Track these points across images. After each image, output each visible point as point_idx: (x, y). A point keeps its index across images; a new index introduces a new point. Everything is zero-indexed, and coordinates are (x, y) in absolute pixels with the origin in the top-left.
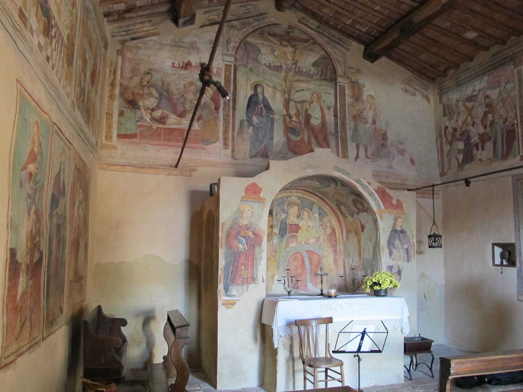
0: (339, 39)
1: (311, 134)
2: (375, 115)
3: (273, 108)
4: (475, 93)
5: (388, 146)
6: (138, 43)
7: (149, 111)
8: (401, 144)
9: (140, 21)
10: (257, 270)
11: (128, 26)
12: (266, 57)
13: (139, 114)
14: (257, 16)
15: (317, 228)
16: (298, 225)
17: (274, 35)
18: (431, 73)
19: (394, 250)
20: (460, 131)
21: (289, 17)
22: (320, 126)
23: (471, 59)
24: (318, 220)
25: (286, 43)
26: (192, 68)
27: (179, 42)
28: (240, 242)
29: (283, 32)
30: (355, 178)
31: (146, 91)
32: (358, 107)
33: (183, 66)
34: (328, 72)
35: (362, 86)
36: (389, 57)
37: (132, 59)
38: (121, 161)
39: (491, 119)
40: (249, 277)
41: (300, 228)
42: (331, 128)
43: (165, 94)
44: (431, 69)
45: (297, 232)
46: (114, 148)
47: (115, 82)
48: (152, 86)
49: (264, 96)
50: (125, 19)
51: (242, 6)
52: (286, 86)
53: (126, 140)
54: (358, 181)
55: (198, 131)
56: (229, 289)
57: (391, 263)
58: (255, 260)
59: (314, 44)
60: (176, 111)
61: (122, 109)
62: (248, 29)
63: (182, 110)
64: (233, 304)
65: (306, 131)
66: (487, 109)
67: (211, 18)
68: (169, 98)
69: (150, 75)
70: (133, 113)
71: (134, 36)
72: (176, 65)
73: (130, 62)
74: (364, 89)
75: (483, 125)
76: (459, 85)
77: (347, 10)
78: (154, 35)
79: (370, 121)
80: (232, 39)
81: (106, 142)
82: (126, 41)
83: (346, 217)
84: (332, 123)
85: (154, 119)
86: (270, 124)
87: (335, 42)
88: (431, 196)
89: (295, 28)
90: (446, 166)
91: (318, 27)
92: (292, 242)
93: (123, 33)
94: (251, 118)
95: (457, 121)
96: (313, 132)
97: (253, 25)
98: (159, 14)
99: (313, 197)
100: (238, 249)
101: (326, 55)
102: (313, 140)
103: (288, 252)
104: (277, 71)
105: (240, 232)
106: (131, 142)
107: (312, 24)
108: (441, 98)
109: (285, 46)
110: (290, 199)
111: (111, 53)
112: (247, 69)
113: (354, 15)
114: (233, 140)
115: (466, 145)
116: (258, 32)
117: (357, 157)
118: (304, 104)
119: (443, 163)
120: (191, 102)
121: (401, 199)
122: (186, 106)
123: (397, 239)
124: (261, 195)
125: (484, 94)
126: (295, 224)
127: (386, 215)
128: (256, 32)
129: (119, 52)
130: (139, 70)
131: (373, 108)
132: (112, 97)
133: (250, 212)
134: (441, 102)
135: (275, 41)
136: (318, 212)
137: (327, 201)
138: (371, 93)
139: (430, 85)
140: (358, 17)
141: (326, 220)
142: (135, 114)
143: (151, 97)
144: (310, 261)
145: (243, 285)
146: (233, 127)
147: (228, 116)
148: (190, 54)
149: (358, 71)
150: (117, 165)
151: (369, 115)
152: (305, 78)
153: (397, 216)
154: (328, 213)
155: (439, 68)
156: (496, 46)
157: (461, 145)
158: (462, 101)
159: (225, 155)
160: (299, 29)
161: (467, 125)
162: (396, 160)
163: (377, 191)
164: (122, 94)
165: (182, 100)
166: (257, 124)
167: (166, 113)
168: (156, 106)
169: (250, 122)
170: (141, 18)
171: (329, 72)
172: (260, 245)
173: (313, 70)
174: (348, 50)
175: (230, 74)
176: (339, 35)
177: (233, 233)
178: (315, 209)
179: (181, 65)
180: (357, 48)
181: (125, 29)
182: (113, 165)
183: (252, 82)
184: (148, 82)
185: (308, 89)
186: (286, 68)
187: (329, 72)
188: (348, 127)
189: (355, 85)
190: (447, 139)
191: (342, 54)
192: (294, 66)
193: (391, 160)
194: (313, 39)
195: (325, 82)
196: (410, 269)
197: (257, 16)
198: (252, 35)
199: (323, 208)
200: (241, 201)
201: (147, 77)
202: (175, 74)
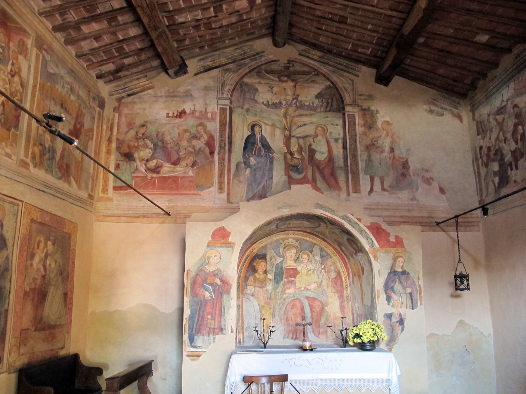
0: (346, 66)
1: (316, 169)
2: (393, 142)
3: (272, 147)
4: (504, 104)
5: (410, 175)
6: (133, 98)
7: (144, 162)
8: (427, 171)
9: (135, 78)
11: (126, 83)
12: (264, 95)
13: (134, 165)
14: (254, 55)
15: (319, 272)
16: (296, 269)
18: (458, 86)
19: (393, 295)
20: (493, 150)
21: (290, 52)
22: (327, 160)
23: (496, 65)
24: (319, 263)
25: (285, 78)
26: (187, 115)
27: (173, 92)
29: (281, 68)
30: (341, 214)
31: (141, 143)
32: (371, 136)
33: (177, 115)
35: (375, 112)
36: (405, 75)
37: (128, 114)
38: (116, 212)
39: (522, 131)
40: (216, 327)
41: (298, 273)
42: (339, 162)
43: (160, 144)
44: (456, 84)
45: (295, 277)
46: (110, 199)
47: (111, 138)
48: (147, 138)
49: (262, 135)
50: (119, 78)
51: (238, 48)
52: (287, 123)
53: (121, 191)
54: (345, 218)
55: (192, 177)
56: (195, 340)
57: (389, 310)
58: (223, 309)
59: (317, 75)
60: (170, 159)
62: (244, 70)
63: (177, 157)
64: (199, 356)
66: (516, 121)
67: (206, 64)
68: (164, 147)
70: (128, 165)
71: (130, 92)
72: (171, 114)
73: (126, 117)
75: (514, 141)
76: (488, 97)
77: (342, 35)
79: (387, 149)
80: (228, 82)
81: (103, 195)
82: (123, 98)
83: (350, 259)
84: (341, 156)
85: (148, 170)
87: (342, 70)
88: (455, 228)
89: (294, 61)
90: (484, 194)
91: (321, 57)
92: (289, 288)
93: (121, 91)
95: (490, 139)
96: (318, 168)
97: (249, 65)
98: (153, 68)
99: (313, 238)
100: (204, 297)
101: (332, 85)
103: (285, 299)
104: (276, 108)
105: (206, 279)
106: (126, 194)
107: (314, 55)
108: (473, 114)
109: (284, 81)
110: (286, 241)
111: (108, 110)
112: (243, 110)
113: (350, 38)
114: (229, 183)
115: (500, 166)
116: (256, 70)
117: (371, 190)
118: (307, 139)
119: (481, 190)
120: (186, 149)
121: (402, 235)
123: (397, 282)
124: (230, 239)
125: (512, 103)
126: (292, 269)
127: (381, 255)
128: (253, 72)
130: (134, 124)
131: (390, 134)
132: (108, 152)
133: (217, 257)
134: (474, 119)
137: (329, 241)
138: (388, 119)
139: (462, 102)
140: (355, 40)
142: (130, 166)
143: (146, 148)
144: (311, 309)
145: (209, 336)
146: (229, 170)
147: (224, 159)
148: (184, 102)
149: (370, 97)
150: (112, 216)
151: (386, 143)
152: (307, 112)
153: (396, 255)
154: (332, 255)
155: (466, 81)
156: (518, 45)
157: (495, 166)
158: (492, 115)
159: (219, 199)
160: (300, 63)
161: (500, 142)
162: (420, 190)
163: (369, 228)
164: (118, 148)
165: (176, 148)
166: (254, 165)
167: (160, 163)
168: (151, 156)
169: (247, 164)
170: (135, 75)
172: (228, 292)
173: (316, 102)
174: (358, 76)
175: (225, 117)
176: (345, 62)
177: (199, 280)
178: (316, 250)
179: (176, 114)
180: (367, 73)
181: (122, 87)
182: (109, 216)
183: (249, 123)
184: (143, 134)
185: (312, 123)
186: (286, 104)
188: (359, 158)
189: (367, 113)
190: (483, 161)
191: (350, 82)
192: (295, 101)
193: (414, 190)
195: (331, 113)
196: (416, 319)
197: (254, 55)
198: (248, 75)
199: (326, 249)
200: (208, 246)
201: (142, 129)
202: (170, 124)
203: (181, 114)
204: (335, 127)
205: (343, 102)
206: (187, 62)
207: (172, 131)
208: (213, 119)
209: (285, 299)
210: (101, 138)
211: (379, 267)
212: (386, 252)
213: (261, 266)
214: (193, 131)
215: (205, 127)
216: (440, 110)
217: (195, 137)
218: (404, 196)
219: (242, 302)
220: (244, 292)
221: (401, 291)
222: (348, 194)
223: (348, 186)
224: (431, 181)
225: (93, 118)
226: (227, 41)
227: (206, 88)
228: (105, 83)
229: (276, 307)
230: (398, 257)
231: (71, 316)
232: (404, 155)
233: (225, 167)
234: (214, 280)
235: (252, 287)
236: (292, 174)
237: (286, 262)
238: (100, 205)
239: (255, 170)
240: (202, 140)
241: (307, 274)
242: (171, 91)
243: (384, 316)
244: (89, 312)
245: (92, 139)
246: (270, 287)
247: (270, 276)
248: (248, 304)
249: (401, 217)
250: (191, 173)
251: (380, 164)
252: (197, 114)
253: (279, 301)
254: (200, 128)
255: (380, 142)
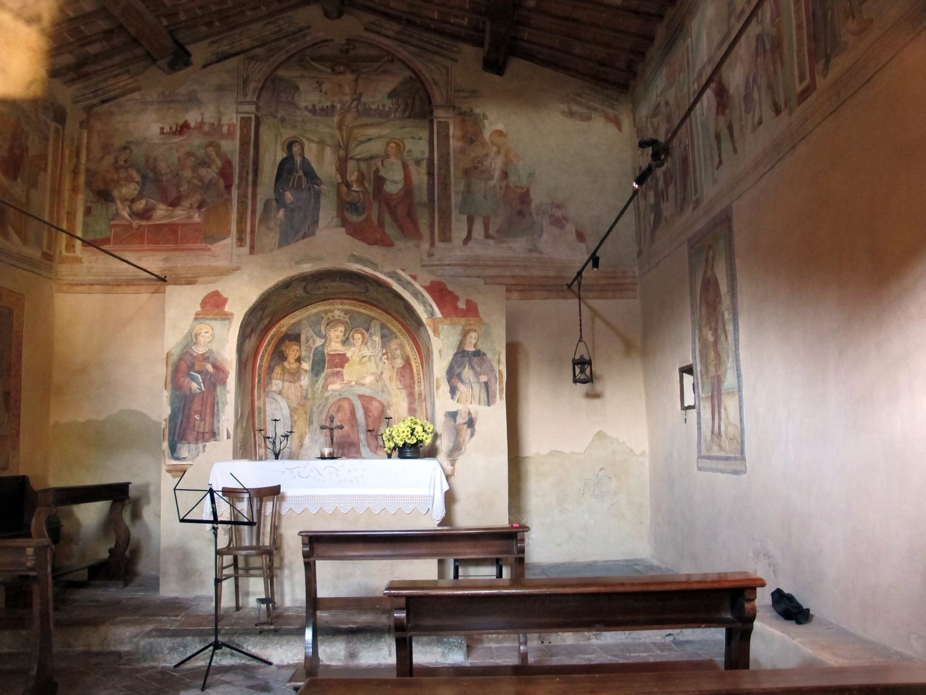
0: (437, 46)
2: (508, 162)
3: (318, 175)
5: (531, 214)
7: (127, 203)
8: (559, 207)
10: (219, 421)
12: (308, 97)
14: (294, 33)
15: (378, 359)
16: (344, 355)
17: (320, 59)
19: (460, 385)
21: (351, 25)
24: (379, 347)
25: (342, 68)
28: (194, 379)
30: (387, 270)
31: (123, 174)
32: (473, 155)
34: (418, 103)
38: (88, 278)
42: (421, 195)
43: (151, 175)
45: (342, 367)
46: (79, 260)
48: (132, 166)
50: (86, 76)
52: (342, 138)
54: (393, 275)
55: (198, 224)
57: (453, 406)
59: (392, 61)
61: (89, 204)
65: (376, 206)
69: (128, 151)
74: (486, 122)
78: (133, 90)
79: (497, 174)
82: (94, 105)
84: (425, 187)
85: (135, 215)
86: (313, 200)
87: (430, 51)
89: (356, 41)
92: (334, 383)
94: (283, 195)
96: (388, 205)
99: (371, 310)
100: (190, 389)
101: (414, 76)
102: (387, 218)
103: (327, 399)
105: (193, 365)
108: (634, 116)
109: (340, 73)
110: (330, 315)
111: (71, 126)
114: (252, 232)
118: (373, 162)
120: (189, 182)
121: (476, 298)
122: (182, 189)
124: (227, 308)
127: (445, 328)
129: (83, 124)
130: (112, 145)
131: (503, 152)
132: (74, 190)
135: (322, 68)
136: (379, 333)
138: (500, 127)
141: (393, 345)
142: (107, 208)
145: (197, 443)
146: (254, 212)
147: (246, 196)
148: (187, 110)
149: (474, 94)
150: (82, 285)
151: (496, 165)
152: (375, 120)
153: (468, 328)
154: (398, 334)
162: (545, 236)
163: (428, 289)
164: (88, 184)
166: (292, 203)
171: (417, 103)
172: (224, 383)
173: (389, 104)
175: (249, 132)
177: (184, 366)
180: (470, 55)
182: (77, 285)
183: (284, 139)
184: (125, 161)
187: (417, 103)
188: (453, 189)
189: (467, 118)
193: (535, 237)
194: (389, 53)
199: (389, 325)
200: (196, 319)
203: (183, 128)
204: (418, 144)
205: (430, 102)
206: (189, 48)
207: (169, 155)
208: (230, 135)
209: (327, 399)
210: (61, 169)
211: (441, 345)
212: (452, 324)
213: (292, 352)
214: (200, 153)
215: (217, 147)
216: (585, 111)
217: (204, 163)
218: (518, 246)
219: (265, 404)
220: (267, 389)
221: (471, 379)
222: (432, 244)
223: (432, 232)
224: (564, 222)
225: (46, 139)
226: (249, 13)
227: (221, 88)
228: (65, 83)
229: (314, 409)
230: (469, 331)
231: (19, 425)
232: (525, 182)
233: (247, 208)
234: (204, 366)
235: (279, 383)
236: (348, 215)
237: (330, 345)
238: (64, 270)
239: (292, 210)
240: (214, 167)
241: (360, 363)
242: (167, 93)
243: (445, 415)
244: (51, 424)
245: (46, 172)
246: (305, 381)
247: (306, 366)
248: (273, 406)
249: (513, 277)
250: (197, 218)
251: (485, 197)
252: (206, 128)
253: (318, 402)
254: (210, 149)
255: (487, 163)
